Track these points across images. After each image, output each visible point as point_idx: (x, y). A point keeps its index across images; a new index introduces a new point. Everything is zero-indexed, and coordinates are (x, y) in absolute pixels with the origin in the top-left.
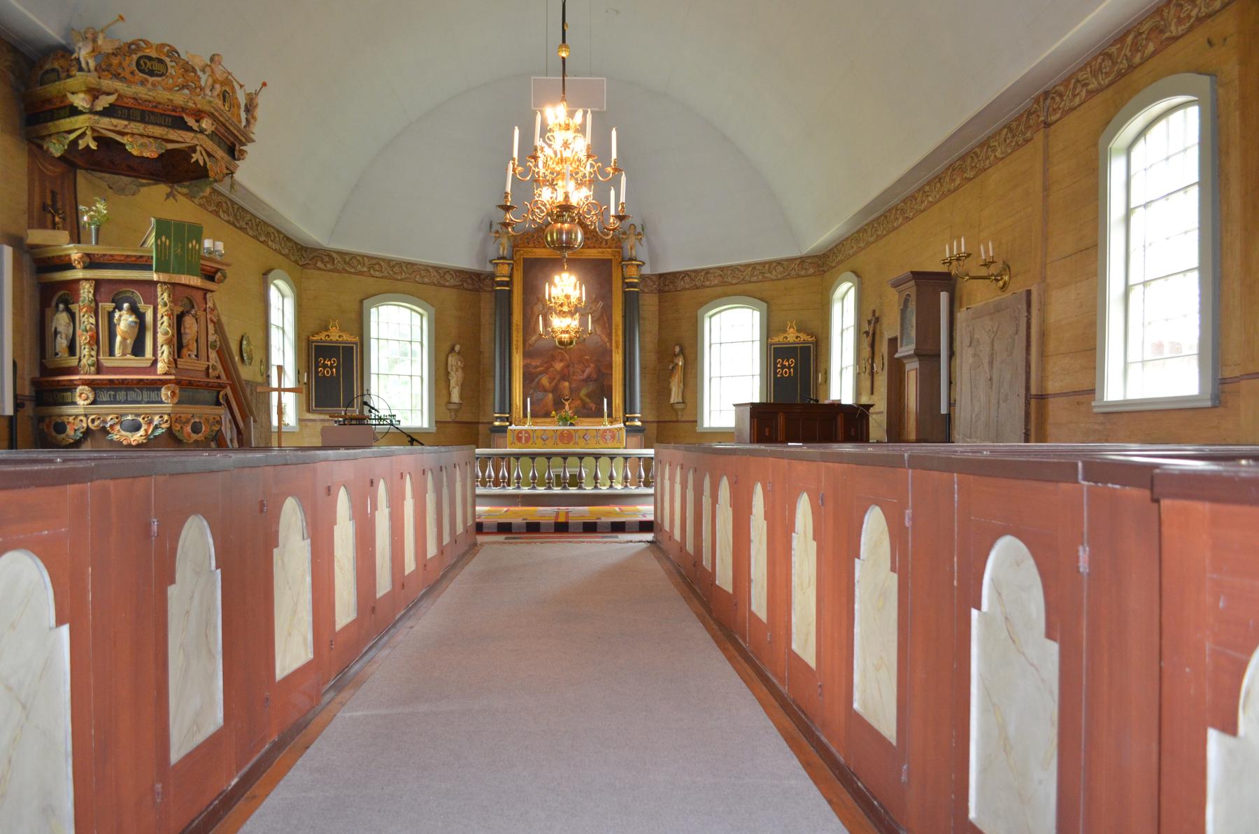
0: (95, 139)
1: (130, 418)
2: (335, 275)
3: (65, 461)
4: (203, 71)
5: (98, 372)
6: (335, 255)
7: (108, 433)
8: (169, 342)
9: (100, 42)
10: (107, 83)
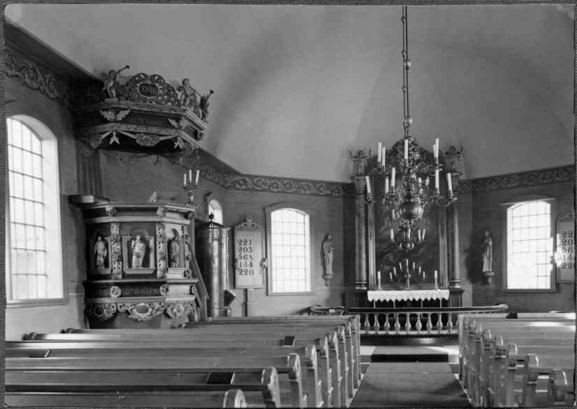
2: (247, 192)
4: (179, 90)
6: (247, 179)
9: (118, 79)
10: (124, 104)
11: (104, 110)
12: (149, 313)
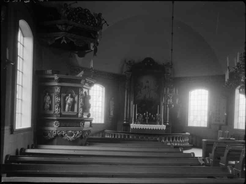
0: (65, 39)
1: (70, 132)
3: (153, 138)
5: (60, 117)
7: (63, 136)
8: (82, 107)
11: (59, 24)
12: (73, 136)
